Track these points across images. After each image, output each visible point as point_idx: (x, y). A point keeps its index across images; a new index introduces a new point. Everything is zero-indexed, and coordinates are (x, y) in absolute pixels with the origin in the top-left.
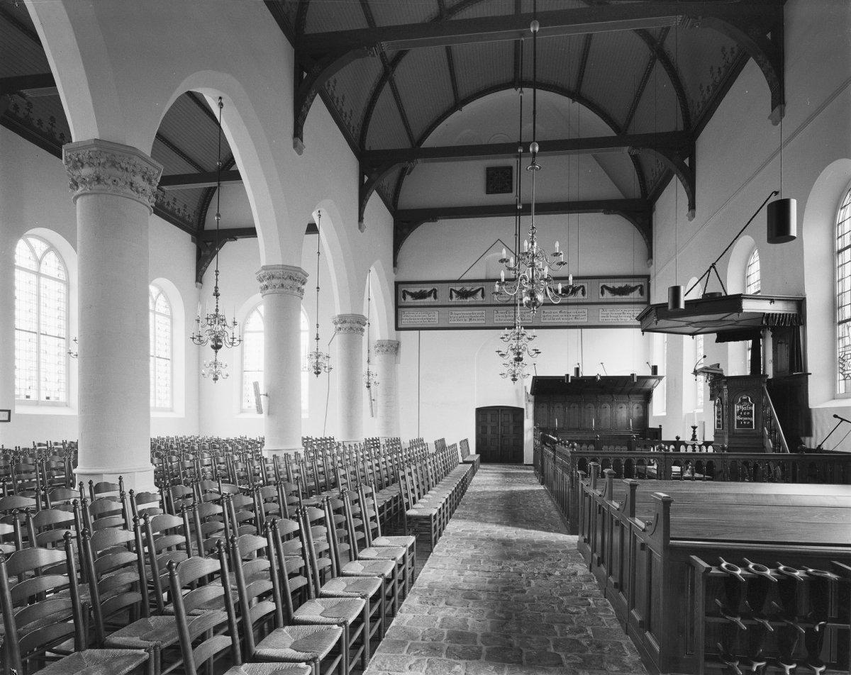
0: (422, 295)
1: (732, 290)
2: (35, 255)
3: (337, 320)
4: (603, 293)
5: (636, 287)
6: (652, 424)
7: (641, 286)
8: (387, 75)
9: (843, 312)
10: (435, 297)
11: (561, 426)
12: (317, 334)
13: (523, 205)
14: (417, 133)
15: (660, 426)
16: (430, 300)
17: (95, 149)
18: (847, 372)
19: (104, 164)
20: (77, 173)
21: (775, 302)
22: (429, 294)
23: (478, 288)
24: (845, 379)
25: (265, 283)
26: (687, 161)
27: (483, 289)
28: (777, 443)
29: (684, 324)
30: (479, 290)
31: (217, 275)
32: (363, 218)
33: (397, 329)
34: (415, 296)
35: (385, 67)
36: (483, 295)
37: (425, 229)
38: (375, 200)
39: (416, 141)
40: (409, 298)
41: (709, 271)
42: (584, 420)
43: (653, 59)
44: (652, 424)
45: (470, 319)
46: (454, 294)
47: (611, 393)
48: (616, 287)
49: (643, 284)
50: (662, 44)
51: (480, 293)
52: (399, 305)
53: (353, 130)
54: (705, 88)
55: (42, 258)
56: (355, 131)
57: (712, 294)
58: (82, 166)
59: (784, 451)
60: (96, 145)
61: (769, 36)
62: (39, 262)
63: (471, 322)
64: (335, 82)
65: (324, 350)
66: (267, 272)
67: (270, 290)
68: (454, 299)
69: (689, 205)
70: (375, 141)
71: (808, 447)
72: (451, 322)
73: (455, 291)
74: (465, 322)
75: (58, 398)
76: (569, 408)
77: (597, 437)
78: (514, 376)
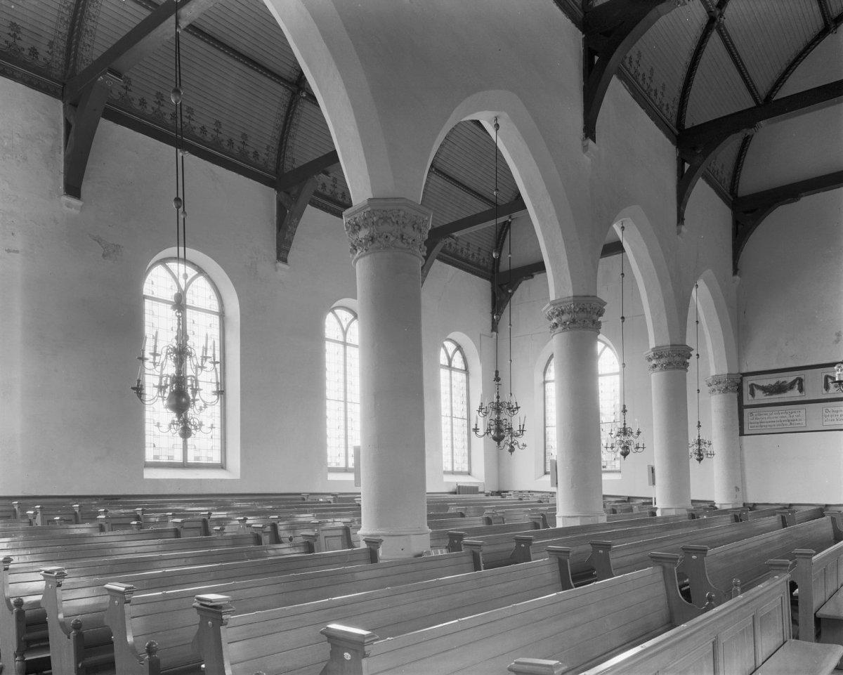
0: (780, 388)
3: (651, 354)
10: (801, 390)
16: (794, 394)
17: (369, 209)
19: (377, 221)
20: (355, 237)
22: (791, 386)
25: (555, 321)
32: (683, 219)
33: (742, 434)
34: (769, 390)
35: (709, 12)
37: (781, 214)
38: (701, 189)
39: (764, 96)
40: (759, 393)
53: (668, 109)
56: (671, 110)
58: (359, 229)
60: (369, 205)
62: (345, 333)
64: (639, 54)
65: (633, 425)
66: (556, 307)
67: (560, 328)
70: (698, 114)
72: (827, 423)
75: (339, 464)
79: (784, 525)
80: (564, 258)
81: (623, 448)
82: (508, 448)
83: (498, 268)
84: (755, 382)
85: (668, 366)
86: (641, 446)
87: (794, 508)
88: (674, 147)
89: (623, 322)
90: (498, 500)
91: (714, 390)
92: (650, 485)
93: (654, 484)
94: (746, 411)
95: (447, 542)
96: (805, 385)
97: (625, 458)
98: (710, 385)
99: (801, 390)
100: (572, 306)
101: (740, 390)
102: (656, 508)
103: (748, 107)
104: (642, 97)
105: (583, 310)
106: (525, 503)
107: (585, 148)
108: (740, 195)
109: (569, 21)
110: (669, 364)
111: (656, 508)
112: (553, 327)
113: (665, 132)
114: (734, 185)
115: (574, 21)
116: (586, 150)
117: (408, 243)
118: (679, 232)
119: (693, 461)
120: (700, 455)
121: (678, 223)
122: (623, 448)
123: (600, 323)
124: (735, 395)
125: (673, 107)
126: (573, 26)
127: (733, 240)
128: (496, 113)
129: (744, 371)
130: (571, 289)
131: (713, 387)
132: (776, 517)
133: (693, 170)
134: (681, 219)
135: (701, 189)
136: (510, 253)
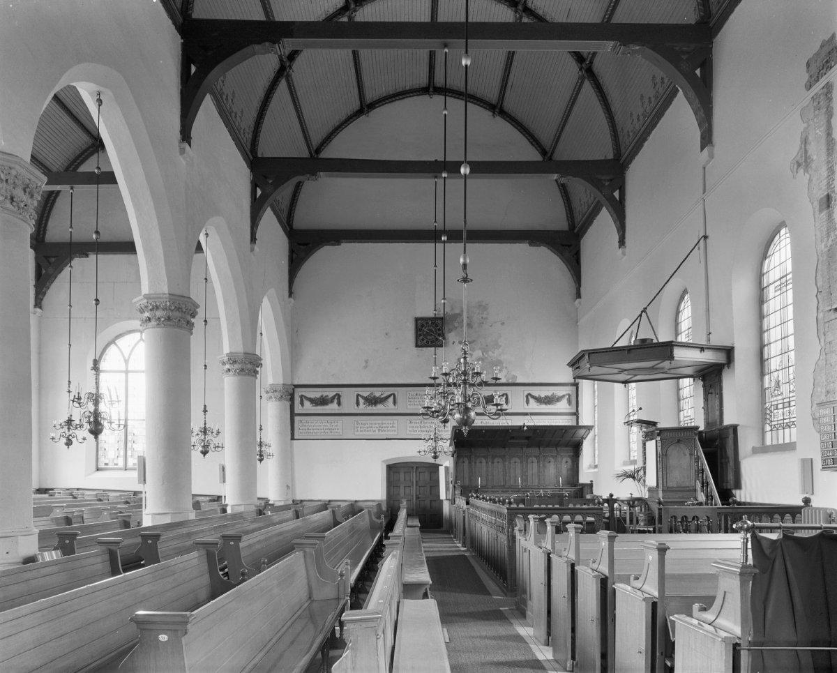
0: (323, 401)
1: (663, 337)
2: (124, 356)
3: (226, 359)
4: (528, 402)
5: (564, 396)
6: (583, 479)
7: (569, 395)
8: (283, 71)
9: (769, 336)
10: (339, 404)
11: (484, 483)
12: (205, 406)
13: (441, 177)
14: (316, 140)
15: (591, 481)
16: (333, 407)
18: (773, 423)
21: (705, 350)
23: (390, 393)
24: (771, 430)
26: (616, 194)
27: (394, 395)
28: (709, 497)
29: (616, 371)
30: (389, 396)
31: (69, 384)
32: (255, 239)
33: (293, 438)
34: (315, 402)
35: (281, 60)
36: (395, 402)
38: (269, 219)
39: (315, 149)
40: (307, 404)
41: (641, 315)
42: (510, 476)
43: (582, 79)
44: (583, 479)
45: (379, 430)
46: (361, 401)
47: (539, 445)
48: (543, 396)
49: (570, 392)
50: (591, 62)
51: (391, 399)
52: (296, 412)
54: (635, 117)
55: (129, 357)
57: (643, 341)
59: (716, 505)
61: (698, 72)
62: (126, 362)
63: (381, 433)
67: (153, 323)
68: (362, 406)
69: (619, 242)
71: (739, 500)
73: (362, 397)
74: (374, 433)
76: (493, 463)
77: (527, 496)
78: (435, 453)
79: (298, 517)
80: (160, 252)
81: (204, 447)
82: (64, 440)
83: (44, 237)
84: (303, 394)
85: (242, 371)
86: (220, 445)
87: (304, 503)
88: (249, 171)
89: (206, 325)
90: (45, 499)
91: (271, 397)
92: (220, 482)
93: (224, 482)
94: (297, 419)
95: (56, 542)
96: (342, 400)
97: (204, 456)
98: (267, 392)
99: (339, 404)
100: (168, 303)
101: (292, 399)
102: (227, 505)
103: (305, 156)
104: (226, 116)
105: (178, 309)
106: (79, 501)
107: (182, 151)
108: (294, 227)
109: (170, 21)
110: (242, 370)
111: (227, 505)
112: (146, 321)
113: (242, 155)
114: (290, 218)
115: (175, 23)
116: (184, 153)
117: (19, 208)
118: (252, 250)
119: (196, 454)
120: (261, 455)
121: (252, 240)
122: (204, 447)
123: (193, 324)
124: (288, 404)
125: (248, 133)
126: (173, 27)
127: (289, 266)
128: (102, 89)
129: (296, 383)
130: (166, 287)
131: (270, 394)
132: (291, 511)
133: (265, 196)
134: (253, 239)
135: (207, 110)
136: (71, 227)
